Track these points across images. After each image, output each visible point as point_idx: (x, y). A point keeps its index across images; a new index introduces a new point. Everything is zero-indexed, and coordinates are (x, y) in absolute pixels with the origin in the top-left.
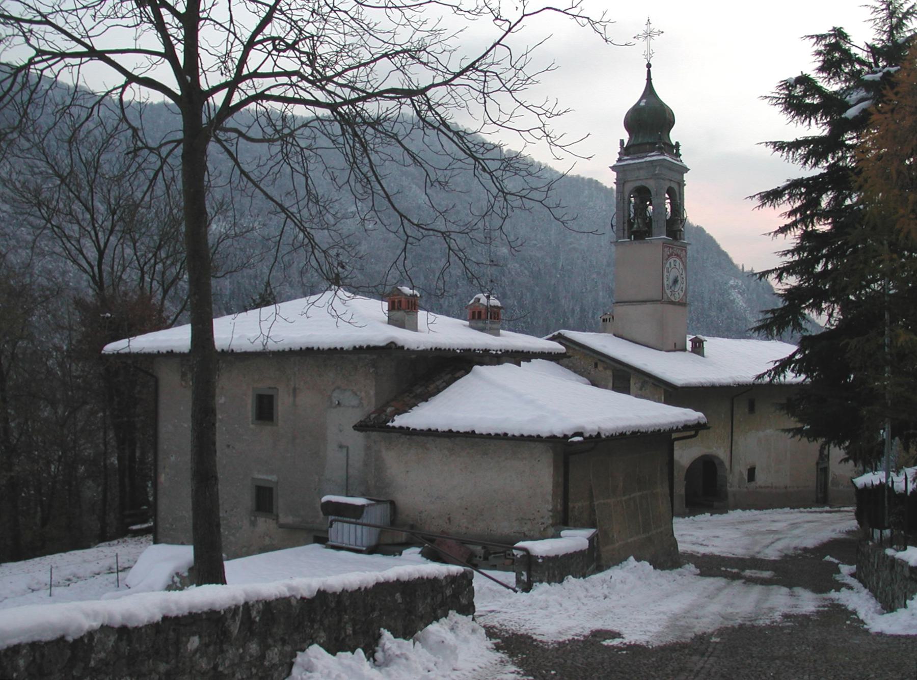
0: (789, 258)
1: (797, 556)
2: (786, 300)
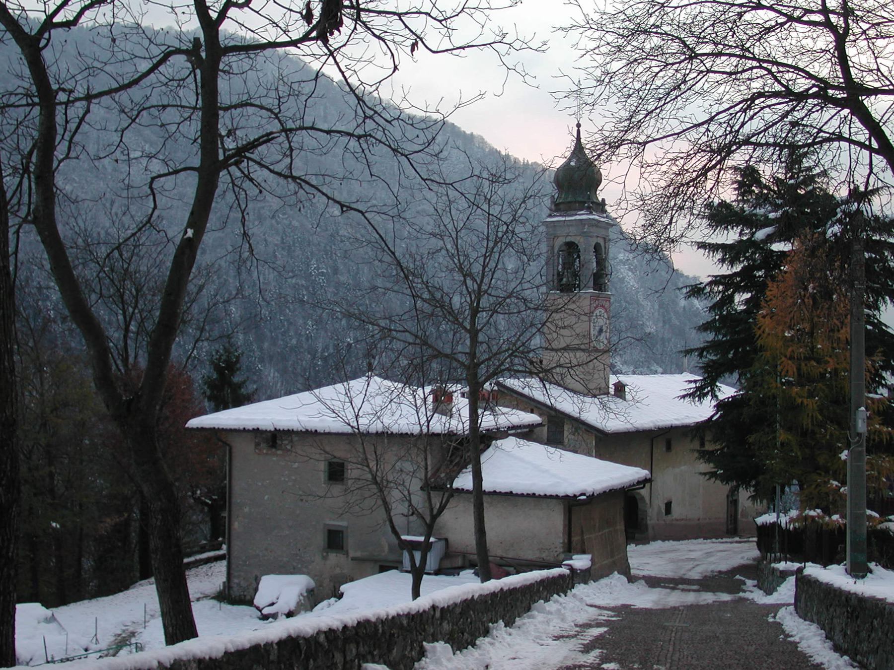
0: (710, 336)
1: (714, 577)
2: (705, 372)
